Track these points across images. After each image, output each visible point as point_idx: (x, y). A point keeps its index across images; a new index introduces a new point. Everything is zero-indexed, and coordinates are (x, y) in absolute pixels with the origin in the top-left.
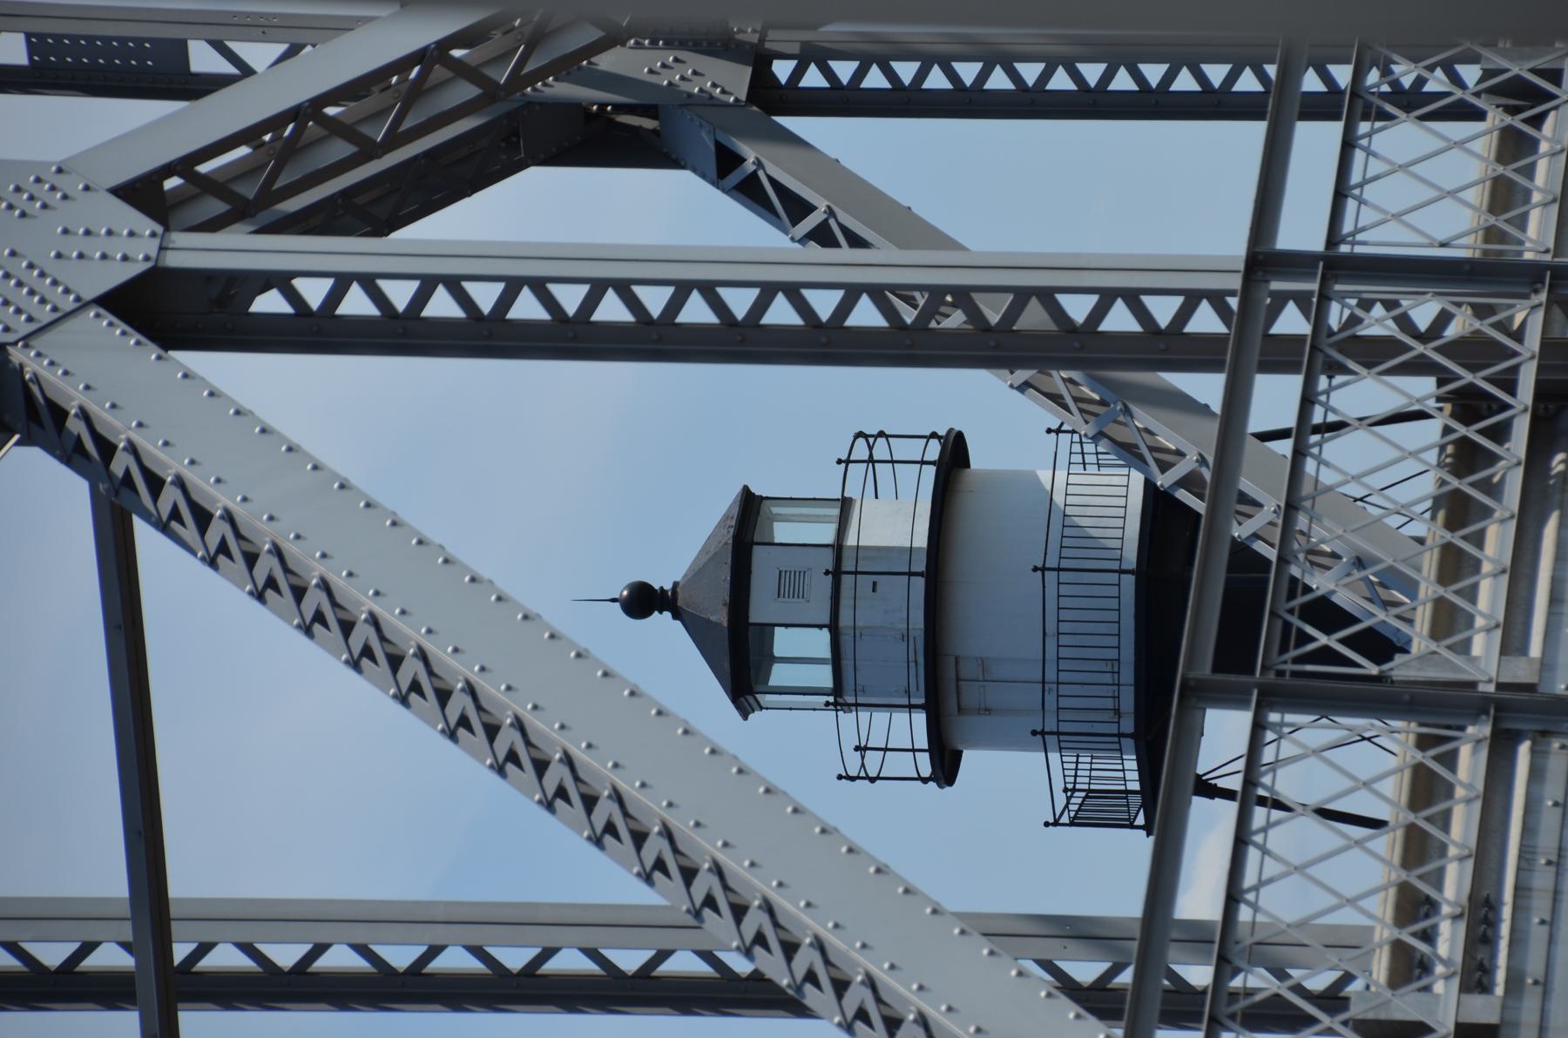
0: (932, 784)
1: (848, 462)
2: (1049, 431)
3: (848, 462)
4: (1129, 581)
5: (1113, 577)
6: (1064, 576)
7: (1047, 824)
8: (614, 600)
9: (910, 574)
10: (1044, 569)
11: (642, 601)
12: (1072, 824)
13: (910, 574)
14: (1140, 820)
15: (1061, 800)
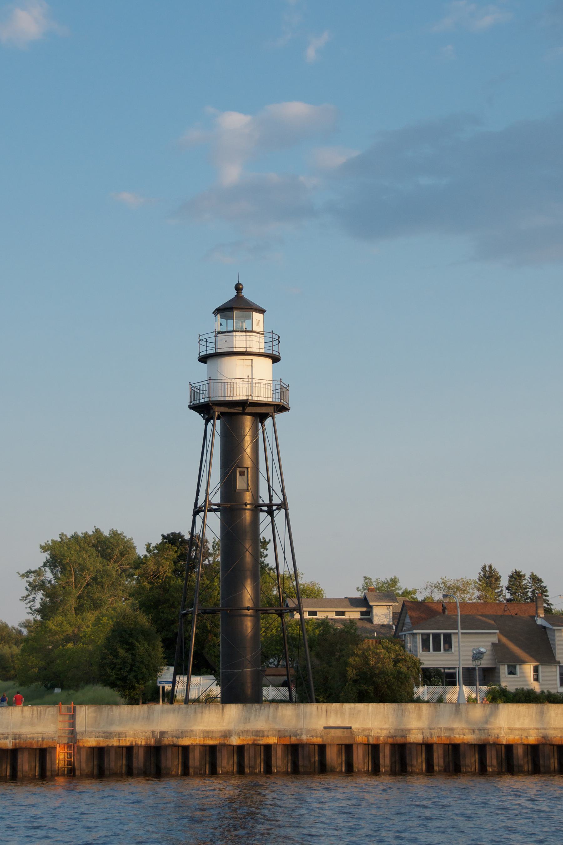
3: (272, 333)
4: (246, 398)
11: (238, 288)
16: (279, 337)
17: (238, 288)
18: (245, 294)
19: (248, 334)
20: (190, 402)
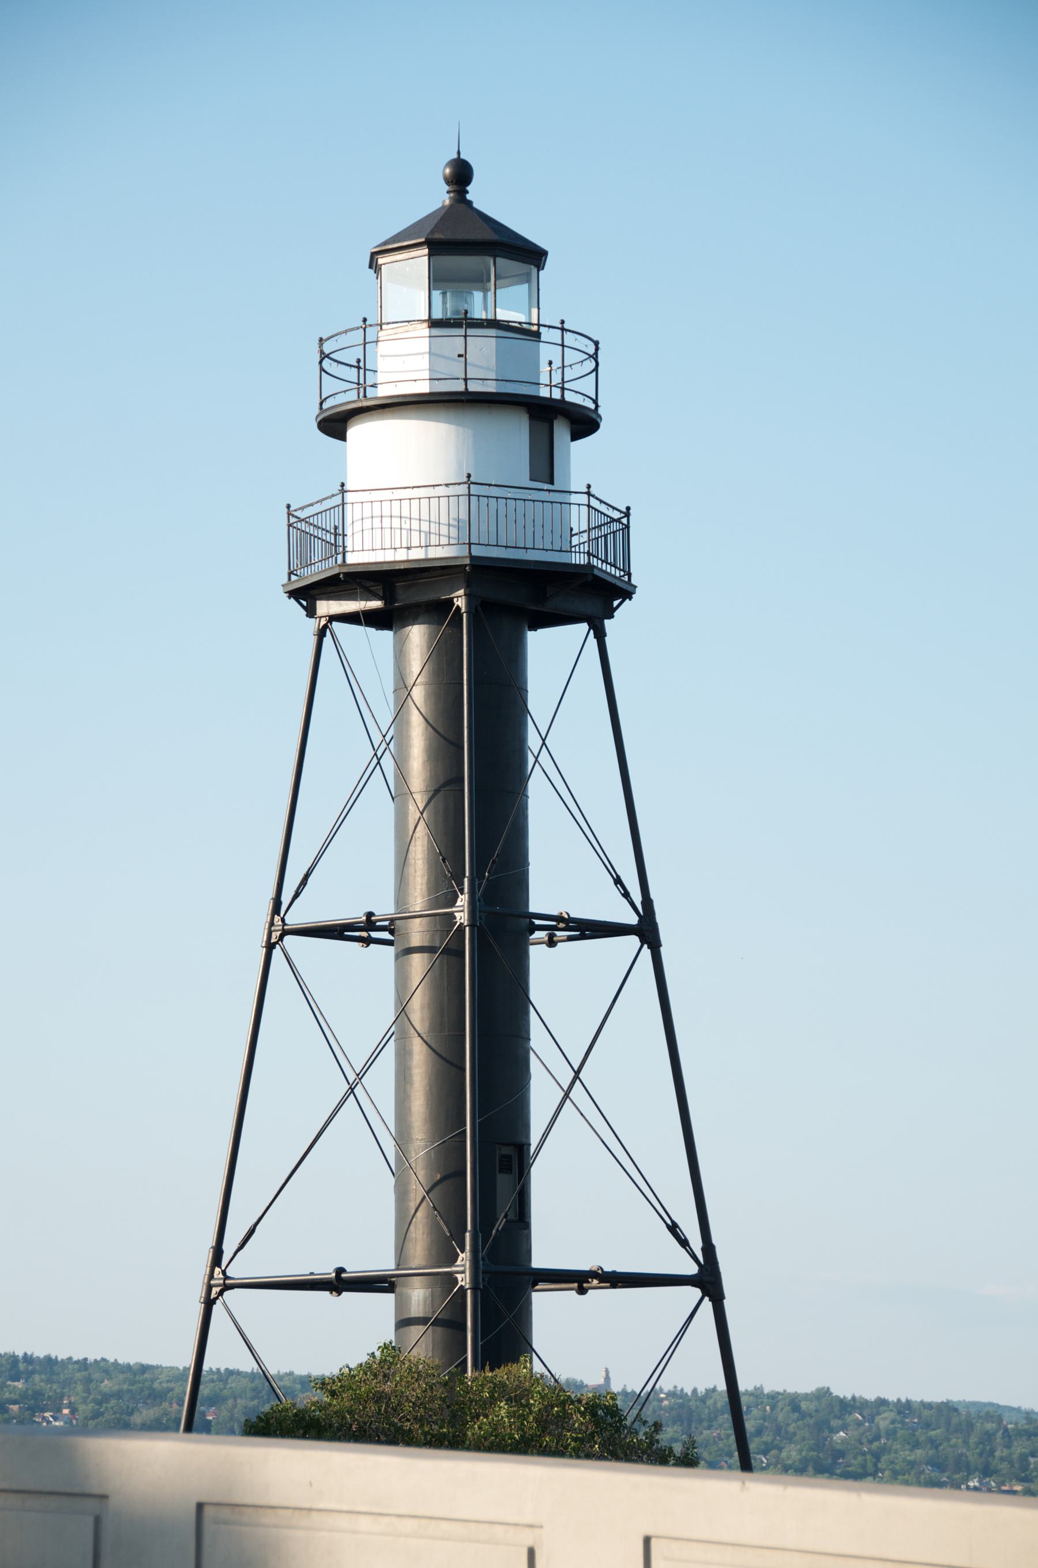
0: (317, 411)
1: (563, 329)
2: (589, 486)
7: (288, 507)
8: (459, 153)
11: (461, 175)
12: (290, 525)
15: (301, 515)
16: (596, 343)
17: (461, 175)
18: (480, 195)
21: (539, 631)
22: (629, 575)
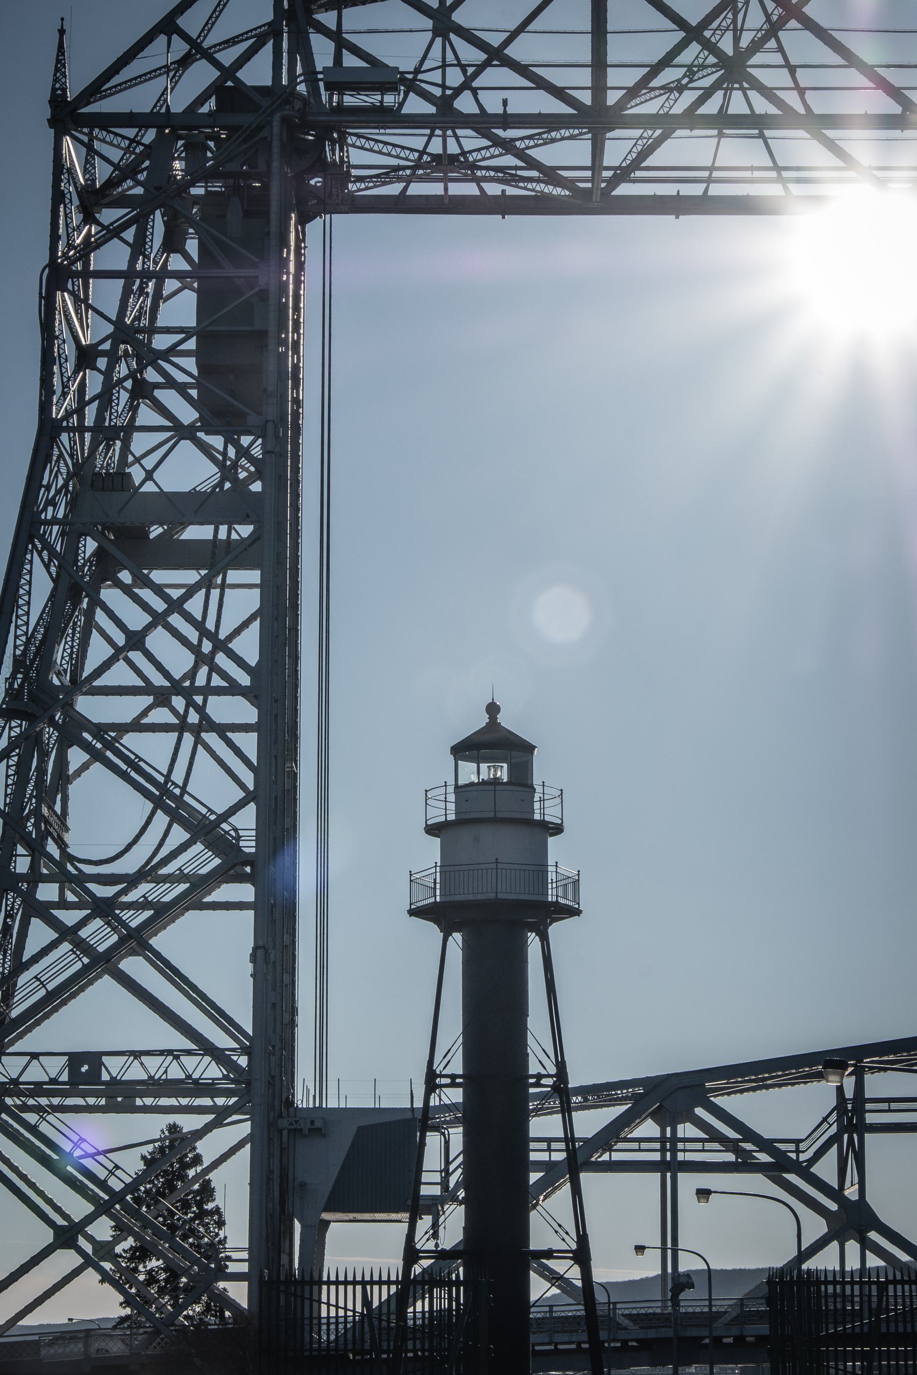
5: (499, 871)
6: (494, 871)
9: (495, 812)
10: (497, 863)
11: (493, 709)
13: (495, 812)
14: (413, 907)
17: (493, 709)
19: (492, 815)
20: (411, 904)
21: (49, 226)
22: (579, 904)
